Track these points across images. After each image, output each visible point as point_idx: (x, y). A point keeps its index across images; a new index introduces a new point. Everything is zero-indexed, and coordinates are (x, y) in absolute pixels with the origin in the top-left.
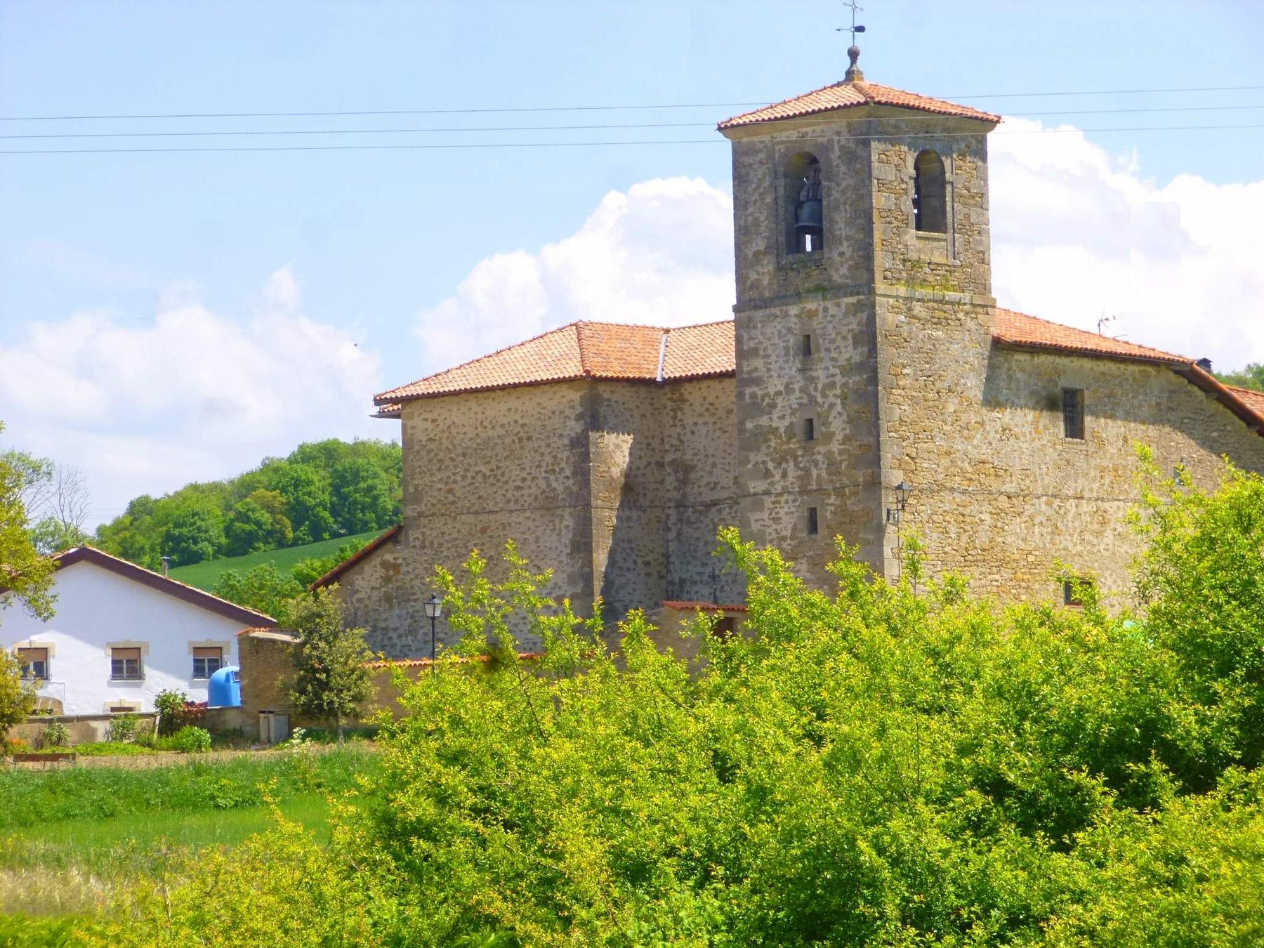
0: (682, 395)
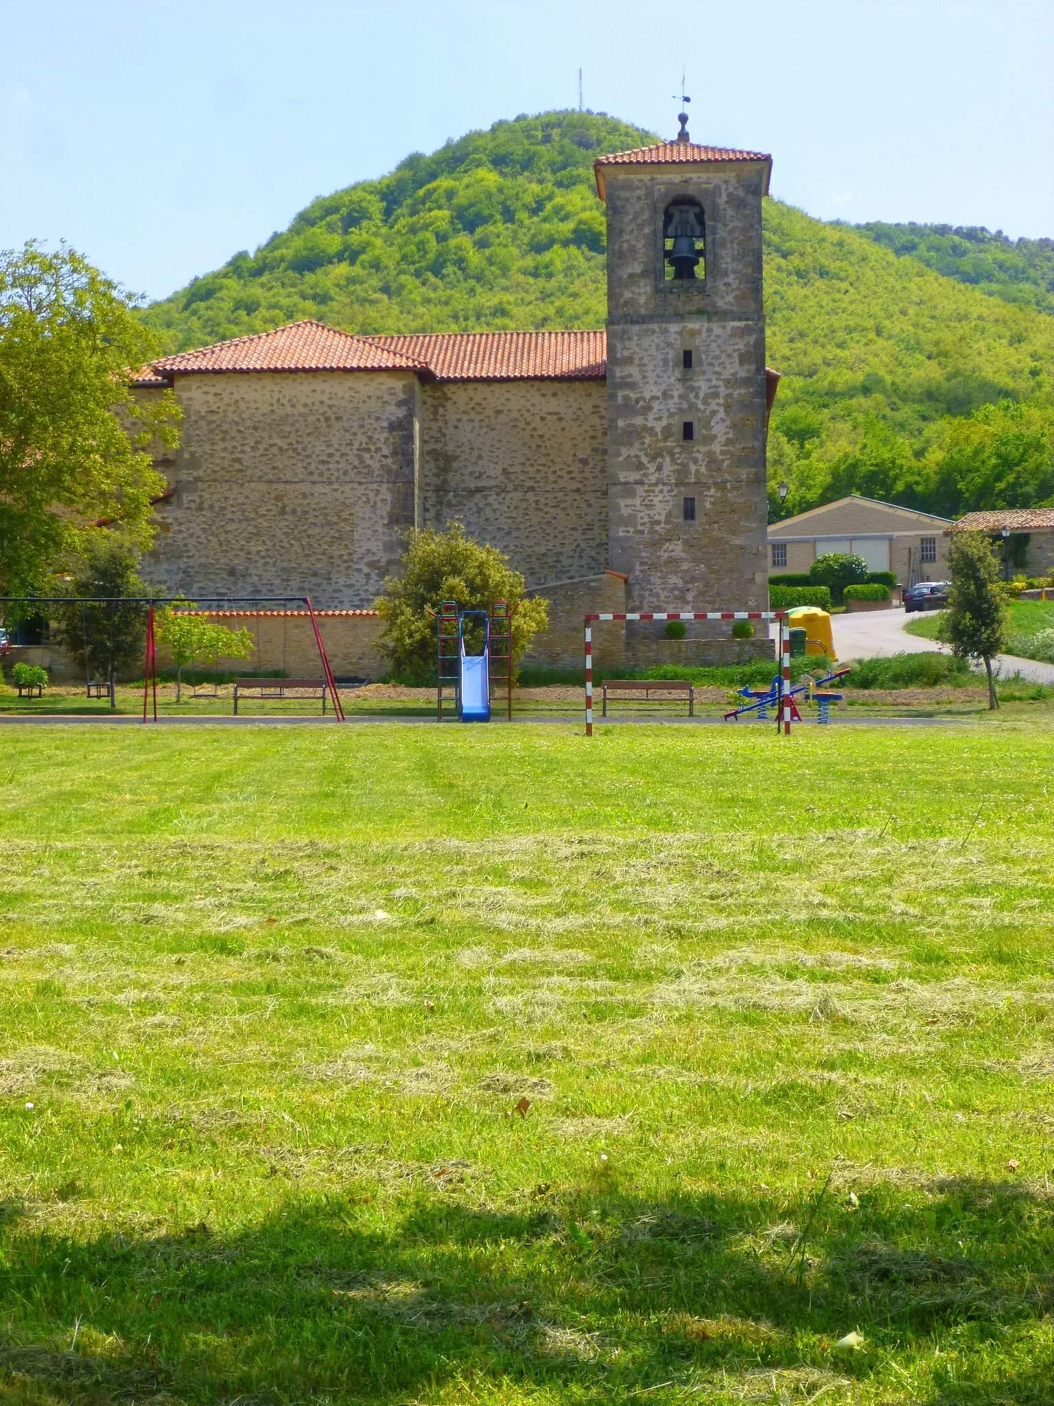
0: (444, 393)
